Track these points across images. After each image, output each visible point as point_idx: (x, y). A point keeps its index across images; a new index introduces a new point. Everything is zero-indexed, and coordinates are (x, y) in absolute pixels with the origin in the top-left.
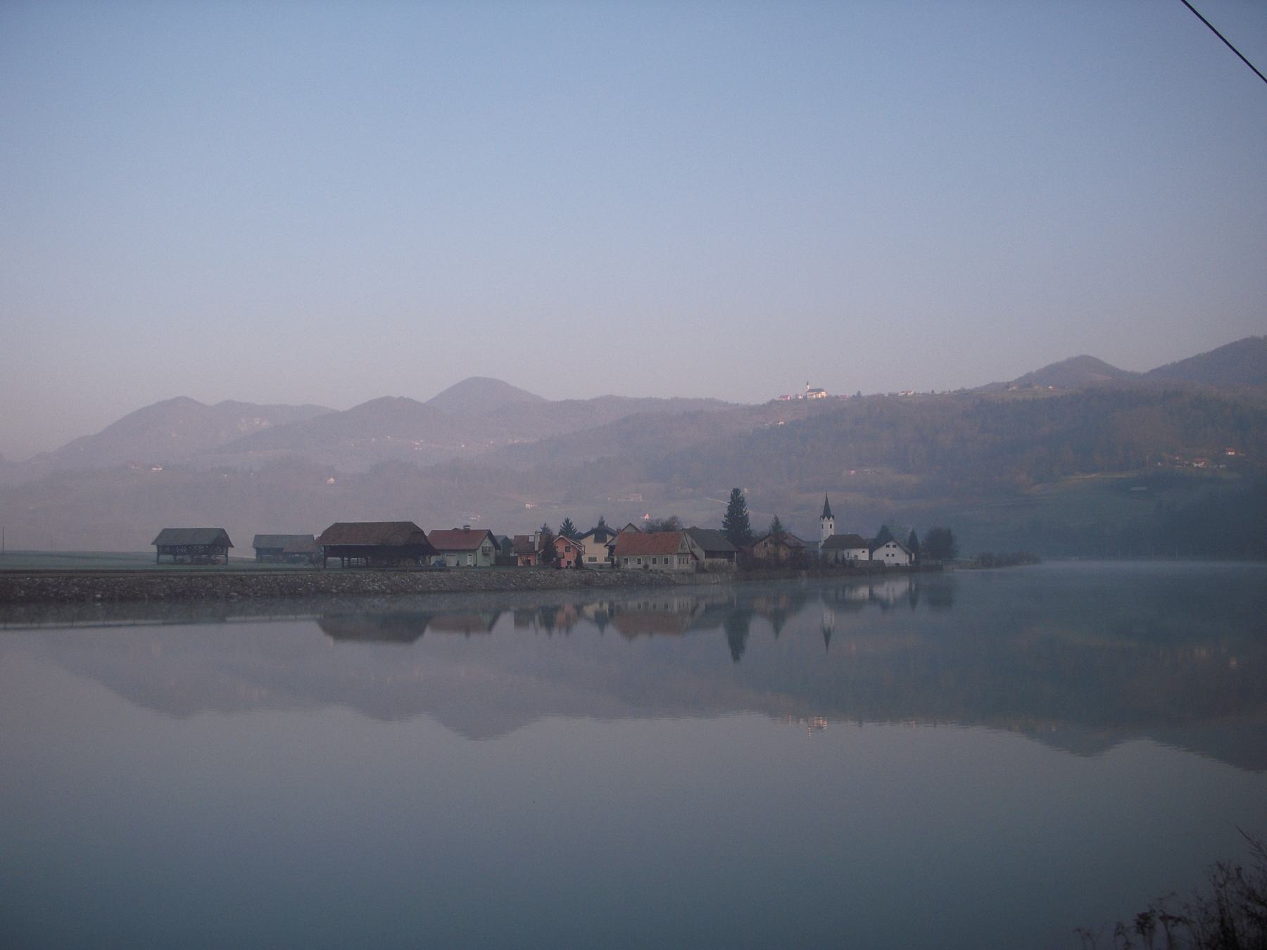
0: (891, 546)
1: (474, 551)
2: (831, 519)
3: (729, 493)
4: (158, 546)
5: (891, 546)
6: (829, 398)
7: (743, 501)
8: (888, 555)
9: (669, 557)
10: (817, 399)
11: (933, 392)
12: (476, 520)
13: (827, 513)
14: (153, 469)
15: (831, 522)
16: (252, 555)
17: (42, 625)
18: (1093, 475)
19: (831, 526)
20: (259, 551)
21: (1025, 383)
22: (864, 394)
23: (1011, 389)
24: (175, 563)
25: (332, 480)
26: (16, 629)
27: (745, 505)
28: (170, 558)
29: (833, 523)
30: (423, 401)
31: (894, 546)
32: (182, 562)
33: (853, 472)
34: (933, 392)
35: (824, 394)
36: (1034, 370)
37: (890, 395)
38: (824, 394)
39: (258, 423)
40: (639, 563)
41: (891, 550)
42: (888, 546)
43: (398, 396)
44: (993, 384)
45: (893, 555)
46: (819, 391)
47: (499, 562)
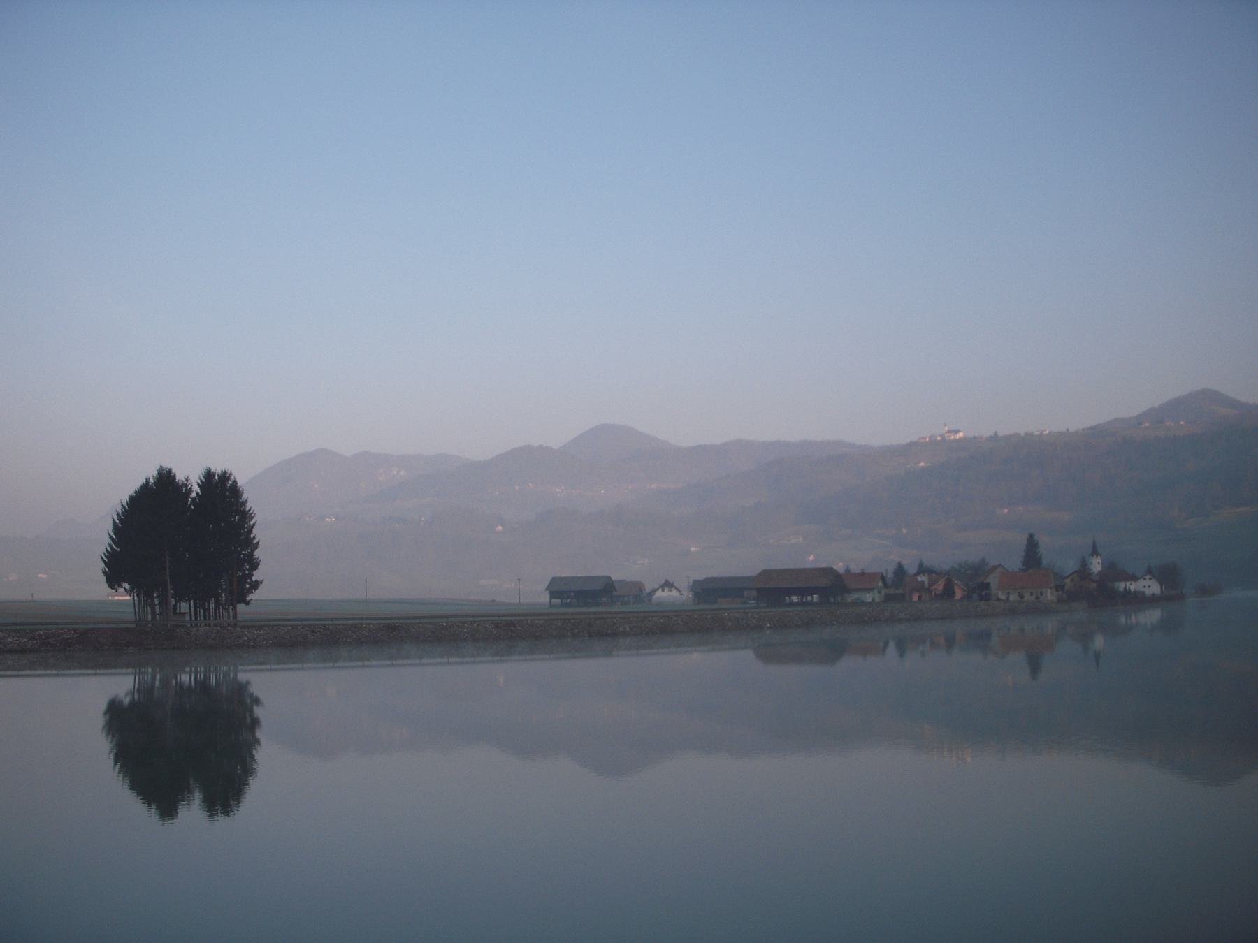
0: (1147, 579)
1: (872, 589)
2: (1099, 557)
3: (1026, 536)
4: (550, 592)
5: (1147, 579)
6: (965, 439)
7: (1037, 544)
8: (1149, 587)
9: (1044, 590)
10: (955, 440)
11: (1067, 430)
12: (643, 564)
13: (1095, 552)
14: (327, 520)
15: (1099, 559)
16: (545, 598)
17: (336, 665)
18: (1243, 509)
19: (1099, 562)
20: (554, 594)
21: (1158, 415)
22: (1001, 434)
23: (1143, 425)
24: (562, 605)
25: (500, 528)
26: (410, 665)
27: (253, 518)
28: (558, 601)
29: (1100, 561)
30: (556, 447)
31: (1150, 579)
32: (569, 605)
33: (1006, 511)
34: (1067, 430)
35: (961, 434)
36: (1156, 405)
37: (1026, 434)
38: (961, 434)
39: (395, 473)
40: (1032, 594)
41: (1147, 583)
42: (1145, 579)
43: (537, 445)
44: (1116, 420)
45: (1145, 587)
46: (957, 432)
47: (889, 598)
